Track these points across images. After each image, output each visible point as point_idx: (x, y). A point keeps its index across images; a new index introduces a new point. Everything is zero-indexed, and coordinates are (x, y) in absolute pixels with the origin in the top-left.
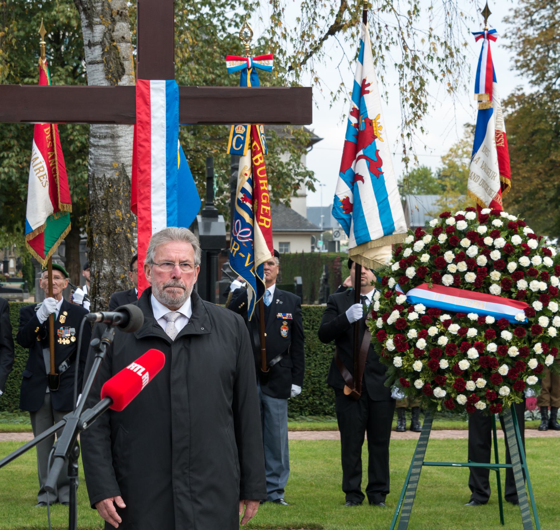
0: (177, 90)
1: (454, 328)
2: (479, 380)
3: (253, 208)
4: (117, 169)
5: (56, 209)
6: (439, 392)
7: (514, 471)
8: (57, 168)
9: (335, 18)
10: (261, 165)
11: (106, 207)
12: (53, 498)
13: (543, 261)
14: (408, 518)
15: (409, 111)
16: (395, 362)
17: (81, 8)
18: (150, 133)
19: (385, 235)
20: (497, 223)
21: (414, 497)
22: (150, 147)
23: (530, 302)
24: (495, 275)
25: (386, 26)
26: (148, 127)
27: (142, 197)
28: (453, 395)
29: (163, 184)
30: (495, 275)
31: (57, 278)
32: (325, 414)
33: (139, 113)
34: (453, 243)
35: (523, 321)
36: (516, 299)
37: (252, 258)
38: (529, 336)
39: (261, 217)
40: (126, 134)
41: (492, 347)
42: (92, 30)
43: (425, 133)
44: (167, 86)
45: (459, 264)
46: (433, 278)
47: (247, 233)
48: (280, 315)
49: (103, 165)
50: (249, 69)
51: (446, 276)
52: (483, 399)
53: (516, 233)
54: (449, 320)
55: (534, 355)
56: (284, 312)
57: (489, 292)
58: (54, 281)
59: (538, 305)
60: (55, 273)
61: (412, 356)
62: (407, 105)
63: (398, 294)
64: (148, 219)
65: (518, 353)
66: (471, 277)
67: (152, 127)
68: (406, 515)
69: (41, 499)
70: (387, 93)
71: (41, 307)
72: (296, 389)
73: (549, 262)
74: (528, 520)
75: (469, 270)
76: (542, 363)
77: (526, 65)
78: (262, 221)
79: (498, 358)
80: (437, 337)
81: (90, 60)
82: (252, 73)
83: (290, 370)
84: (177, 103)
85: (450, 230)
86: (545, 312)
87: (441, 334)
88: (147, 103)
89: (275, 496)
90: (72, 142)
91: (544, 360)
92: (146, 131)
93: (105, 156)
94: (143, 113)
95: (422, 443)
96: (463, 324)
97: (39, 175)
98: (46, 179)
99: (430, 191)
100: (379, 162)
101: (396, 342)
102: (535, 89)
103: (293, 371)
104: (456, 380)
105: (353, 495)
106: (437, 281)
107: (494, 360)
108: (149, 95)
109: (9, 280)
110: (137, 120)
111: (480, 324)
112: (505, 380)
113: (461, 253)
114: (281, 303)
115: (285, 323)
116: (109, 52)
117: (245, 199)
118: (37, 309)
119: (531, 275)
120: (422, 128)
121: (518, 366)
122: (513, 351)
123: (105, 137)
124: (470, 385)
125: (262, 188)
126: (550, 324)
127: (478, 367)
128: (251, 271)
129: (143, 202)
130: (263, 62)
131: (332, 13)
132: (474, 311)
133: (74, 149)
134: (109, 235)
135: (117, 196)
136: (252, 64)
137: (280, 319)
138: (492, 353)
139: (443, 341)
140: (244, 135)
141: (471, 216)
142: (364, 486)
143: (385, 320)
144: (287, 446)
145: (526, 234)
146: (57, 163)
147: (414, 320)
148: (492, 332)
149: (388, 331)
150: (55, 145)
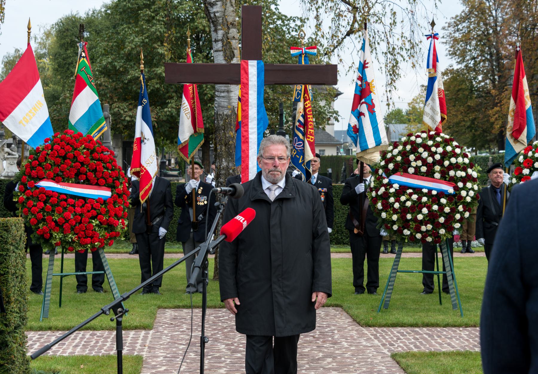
1: (415, 197)
2: (428, 225)
4: (230, 109)
6: (406, 232)
10: (309, 107)
11: (224, 130)
12: (195, 290)
14: (389, 301)
20: (438, 139)
21: (392, 289)
23: (456, 183)
24: (437, 168)
28: (414, 234)
30: (437, 168)
31: (197, 169)
32: (344, 244)
34: (414, 150)
36: (449, 181)
37: (303, 158)
39: (308, 136)
41: (435, 207)
42: (217, 33)
44: (258, 64)
47: (301, 144)
49: (223, 107)
52: (430, 236)
53: (449, 145)
55: (458, 212)
56: (322, 188)
57: (434, 177)
58: (195, 171)
59: (460, 185)
60: (196, 166)
61: (392, 212)
63: (384, 178)
66: (424, 169)
68: (388, 299)
69: (188, 290)
73: (467, 161)
75: (423, 165)
77: (454, 54)
78: (309, 138)
79: (438, 214)
82: (305, 56)
84: (263, 73)
85: (413, 143)
86: (465, 188)
87: (407, 200)
88: (247, 73)
90: (206, 94)
91: (464, 215)
93: (223, 102)
98: (189, 115)
99: (402, 122)
100: (373, 106)
101: (383, 204)
105: (359, 288)
106: (406, 171)
107: (437, 214)
108: (248, 69)
112: (443, 226)
115: (323, 194)
116: (226, 45)
117: (300, 126)
121: (450, 218)
122: (447, 210)
123: (224, 92)
124: (423, 228)
125: (309, 120)
126: (467, 195)
127: (428, 218)
132: (426, 188)
134: (225, 145)
135: (230, 124)
139: (409, 204)
140: (301, 90)
141: (424, 135)
142: (365, 283)
143: (377, 192)
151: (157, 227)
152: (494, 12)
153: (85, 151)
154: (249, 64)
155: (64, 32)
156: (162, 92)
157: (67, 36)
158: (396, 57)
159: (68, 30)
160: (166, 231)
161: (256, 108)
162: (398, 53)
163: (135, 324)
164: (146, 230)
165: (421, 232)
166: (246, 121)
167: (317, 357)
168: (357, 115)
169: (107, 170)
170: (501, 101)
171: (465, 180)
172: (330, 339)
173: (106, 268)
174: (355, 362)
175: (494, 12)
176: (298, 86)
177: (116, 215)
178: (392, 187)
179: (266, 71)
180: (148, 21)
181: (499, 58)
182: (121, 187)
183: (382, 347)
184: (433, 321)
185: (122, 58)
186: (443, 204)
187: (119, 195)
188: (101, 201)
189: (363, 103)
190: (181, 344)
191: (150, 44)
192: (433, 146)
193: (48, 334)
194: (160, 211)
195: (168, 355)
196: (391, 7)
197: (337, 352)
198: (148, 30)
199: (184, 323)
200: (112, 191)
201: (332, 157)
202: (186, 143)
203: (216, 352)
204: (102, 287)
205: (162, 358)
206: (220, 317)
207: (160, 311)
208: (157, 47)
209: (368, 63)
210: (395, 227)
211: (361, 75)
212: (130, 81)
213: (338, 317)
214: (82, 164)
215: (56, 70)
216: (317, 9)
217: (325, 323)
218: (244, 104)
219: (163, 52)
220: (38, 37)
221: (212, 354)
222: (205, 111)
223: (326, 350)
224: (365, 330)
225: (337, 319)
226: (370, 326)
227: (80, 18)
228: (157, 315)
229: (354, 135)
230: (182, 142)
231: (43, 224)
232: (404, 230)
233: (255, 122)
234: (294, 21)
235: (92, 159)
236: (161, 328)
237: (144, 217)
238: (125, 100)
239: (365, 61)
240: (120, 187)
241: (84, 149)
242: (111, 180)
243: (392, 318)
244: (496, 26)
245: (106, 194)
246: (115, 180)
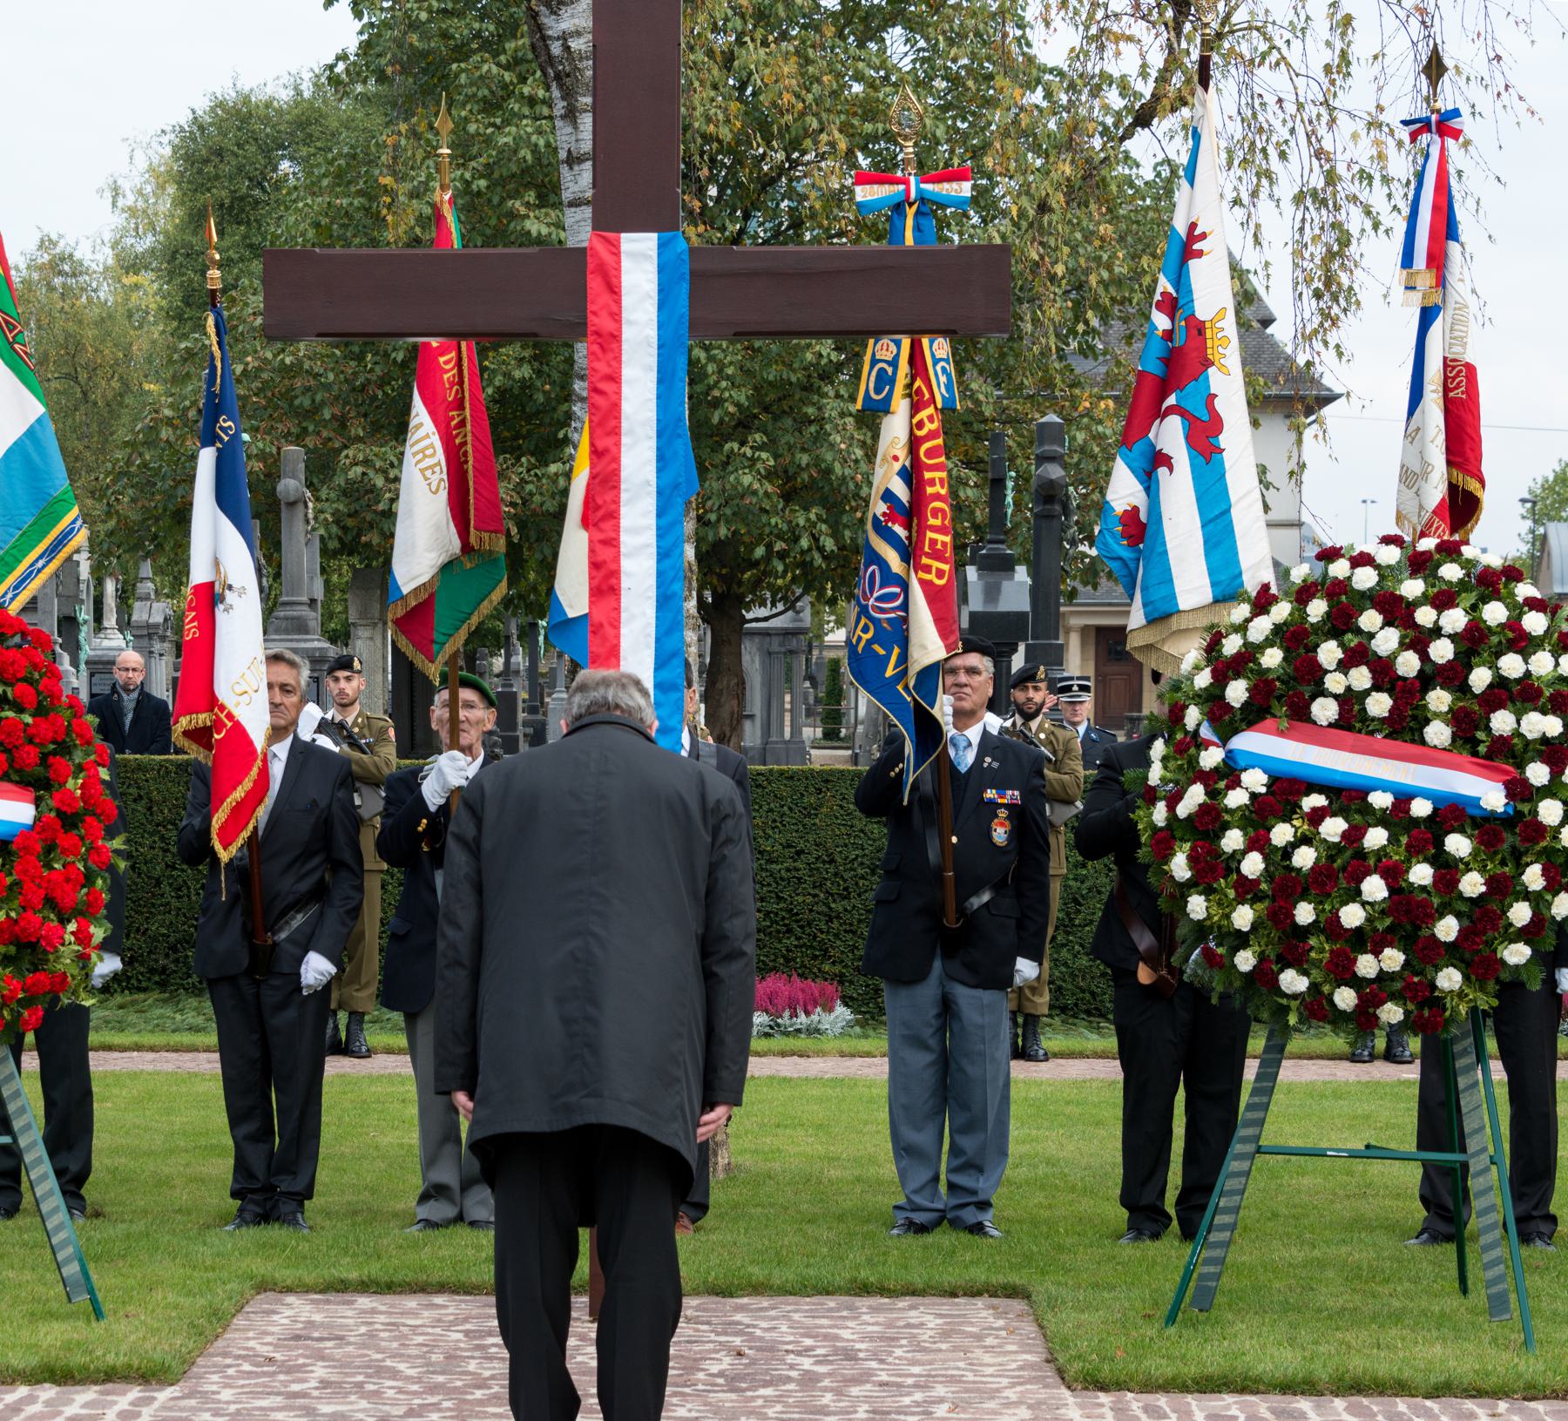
0: (686, 257)
1: (1333, 828)
2: (1388, 952)
3: (909, 538)
5: (466, 547)
6: (1293, 981)
7: (1471, 1170)
8: (469, 448)
9: (1151, 85)
10: (932, 435)
12: (450, 1211)
13: (1557, 664)
14: (1218, 1277)
15: (1310, 305)
16: (1190, 907)
17: (551, 72)
18: (620, 362)
19: (1216, 601)
20: (1451, 572)
21: (1232, 1227)
22: (619, 393)
23: (1521, 766)
25: (1280, 101)
26: (614, 346)
27: (601, 513)
28: (1326, 989)
29: (648, 483)
30: (1439, 699)
31: (469, 705)
33: (594, 313)
34: (1341, 623)
35: (1500, 810)
36: (1489, 756)
37: (904, 658)
38: (1514, 848)
39: (925, 560)
41: (1421, 874)
43: (1344, 359)
45: (1354, 672)
46: (1290, 707)
47: (893, 597)
48: (990, 794)
50: (911, 205)
51: (1320, 700)
52: (1394, 997)
53: (1496, 595)
54: (1323, 808)
56: (1001, 787)
57: (1423, 742)
58: (463, 714)
60: (466, 694)
61: (1231, 893)
62: (1307, 294)
63: (1206, 744)
64: (613, 567)
65: (1483, 889)
66: (1379, 705)
68: (1212, 1269)
69: (423, 1212)
70: (1267, 264)
71: (433, 775)
72: (1026, 969)
74: (1501, 1287)
75: (1377, 687)
76: (1544, 911)
78: (928, 569)
79: (1436, 901)
81: (571, 197)
82: (918, 213)
83: (1013, 922)
84: (685, 287)
85: (1337, 590)
88: (614, 290)
89: (970, 1216)
90: (717, 403)
91: (1549, 905)
92: (610, 355)
94: (604, 313)
95: (1256, 1099)
96: (1357, 818)
97: (422, 465)
98: (440, 476)
100: (1216, 424)
101: (1193, 860)
103: (1020, 926)
104: (1332, 951)
105: (1144, 1214)
106: (1300, 713)
107: (1426, 904)
108: (618, 269)
110: (590, 329)
112: (1452, 953)
113: (1360, 643)
114: (995, 765)
115: (1003, 813)
117: (890, 517)
118: (424, 778)
119: (1524, 701)
120: (1338, 346)
121: (1484, 919)
122: (1472, 884)
124: (1366, 965)
125: (930, 490)
127: (1388, 922)
128: (900, 688)
129: (602, 525)
130: (946, 185)
132: (1384, 786)
133: (721, 421)
136: (919, 190)
137: (992, 802)
138: (1423, 888)
139: (1305, 858)
140: (894, 363)
142: (1171, 1196)
144: (1005, 1099)
145: (1520, 599)
146: (469, 438)
147: (1239, 808)
148: (1424, 837)
149: (1178, 834)
150: (467, 395)
151: (296, 951)
154: (624, 247)
155: (206, 161)
156: (540, 398)
157: (217, 177)
158: (1342, 217)
159: (219, 153)
160: (333, 970)
161: (653, 443)
162: (1354, 199)
163: (111, 1359)
164: (246, 963)
165: (1356, 982)
166: (608, 497)
168: (1143, 464)
173: (17, 1125)
176: (885, 341)
177: (51, 902)
178: (1235, 783)
179: (696, 277)
180: (490, 106)
182: (73, 785)
184: (1384, 1366)
187: (68, 820)
189: (1172, 410)
191: (496, 200)
192: (1425, 599)
194: (305, 886)
198: (488, 141)
200: (37, 802)
202: (424, 596)
204: (82, 1198)
208: (523, 211)
209: (1203, 236)
210: (1245, 961)
211: (1171, 290)
218: (601, 424)
219: (544, 231)
220: (126, 185)
222: (713, 474)
225: (978, 1353)
226: (1103, 1388)
227: (268, 105)
229: (1127, 554)
230: (405, 590)
232: (1282, 971)
233: (650, 503)
236: (215, 1378)
237: (238, 911)
239: (1193, 226)
240: (70, 784)
242: (30, 754)
243: (1207, 1351)
246: (54, 753)
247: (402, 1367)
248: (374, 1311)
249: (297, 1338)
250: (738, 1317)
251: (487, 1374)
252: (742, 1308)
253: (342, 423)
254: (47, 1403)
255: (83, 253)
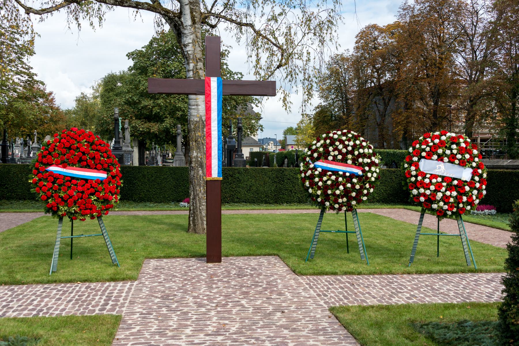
1: (333, 177)
11: (194, 131)
15: (306, 97)
20: (350, 135)
30: (350, 156)
32: (270, 203)
34: (332, 143)
40: (201, 99)
41: (349, 185)
44: (218, 79)
52: (345, 206)
53: (357, 139)
55: (366, 188)
57: (347, 163)
59: (367, 168)
66: (340, 157)
67: (212, 96)
75: (339, 154)
77: (322, 97)
80: (326, 181)
84: (221, 87)
85: (331, 138)
86: (370, 171)
87: (328, 180)
88: (209, 86)
99: (293, 134)
101: (310, 183)
102: (325, 103)
106: (326, 158)
109: (169, 159)
111: (344, 176)
112: (354, 198)
116: (195, 74)
121: (359, 193)
122: (357, 187)
124: (340, 200)
126: (372, 176)
131: (278, 60)
132: (341, 171)
134: (196, 141)
135: (199, 127)
139: (329, 182)
143: (305, 174)
148: (349, 179)
152: (344, 75)
153: (86, 143)
165: (339, 203)
167: (268, 311)
169: (104, 158)
170: (348, 122)
171: (370, 165)
172: (275, 289)
174: (301, 317)
175: (344, 75)
177: (110, 192)
178: (316, 170)
181: (347, 99)
182: (114, 171)
183: (318, 298)
185: (138, 95)
186: (354, 183)
187: (113, 177)
188: (99, 181)
190: (157, 297)
192: (346, 140)
193: (52, 287)
195: (144, 312)
196: (307, 49)
197: (284, 304)
199: (162, 273)
201: (257, 152)
203: (185, 306)
205: (138, 315)
206: (190, 266)
207: (146, 261)
212: (142, 108)
213: (278, 265)
214: (84, 153)
215: (103, 104)
216: (257, 49)
217: (269, 272)
221: (181, 308)
223: (274, 303)
224: (300, 279)
228: (143, 265)
231: (52, 200)
234: (237, 75)
235: (92, 150)
236: (143, 279)
238: (140, 119)
241: (86, 142)
244: (345, 81)
245: (103, 176)
247: (177, 275)
248: (167, 262)
249: (156, 269)
250: (232, 261)
251: (193, 276)
252: (231, 259)
253: (131, 118)
254: (113, 286)
255: (88, 95)
